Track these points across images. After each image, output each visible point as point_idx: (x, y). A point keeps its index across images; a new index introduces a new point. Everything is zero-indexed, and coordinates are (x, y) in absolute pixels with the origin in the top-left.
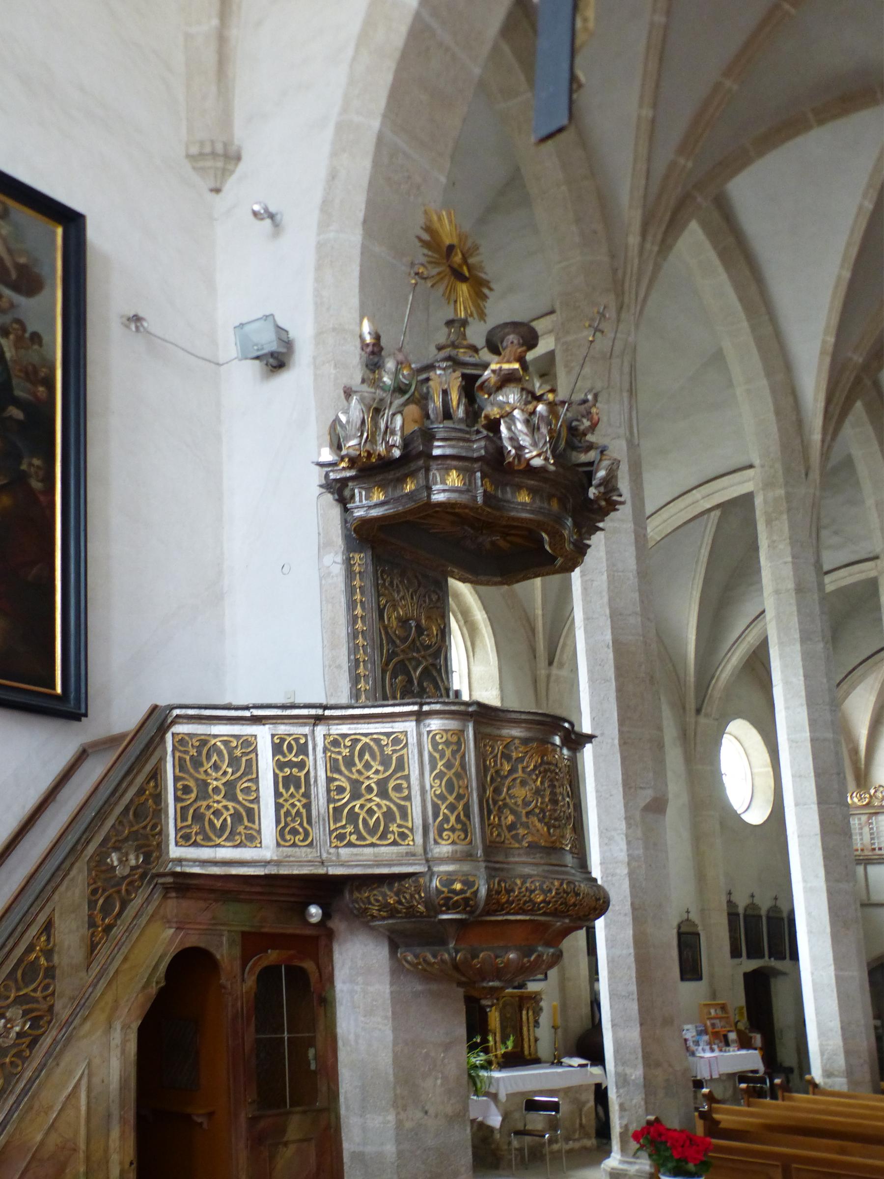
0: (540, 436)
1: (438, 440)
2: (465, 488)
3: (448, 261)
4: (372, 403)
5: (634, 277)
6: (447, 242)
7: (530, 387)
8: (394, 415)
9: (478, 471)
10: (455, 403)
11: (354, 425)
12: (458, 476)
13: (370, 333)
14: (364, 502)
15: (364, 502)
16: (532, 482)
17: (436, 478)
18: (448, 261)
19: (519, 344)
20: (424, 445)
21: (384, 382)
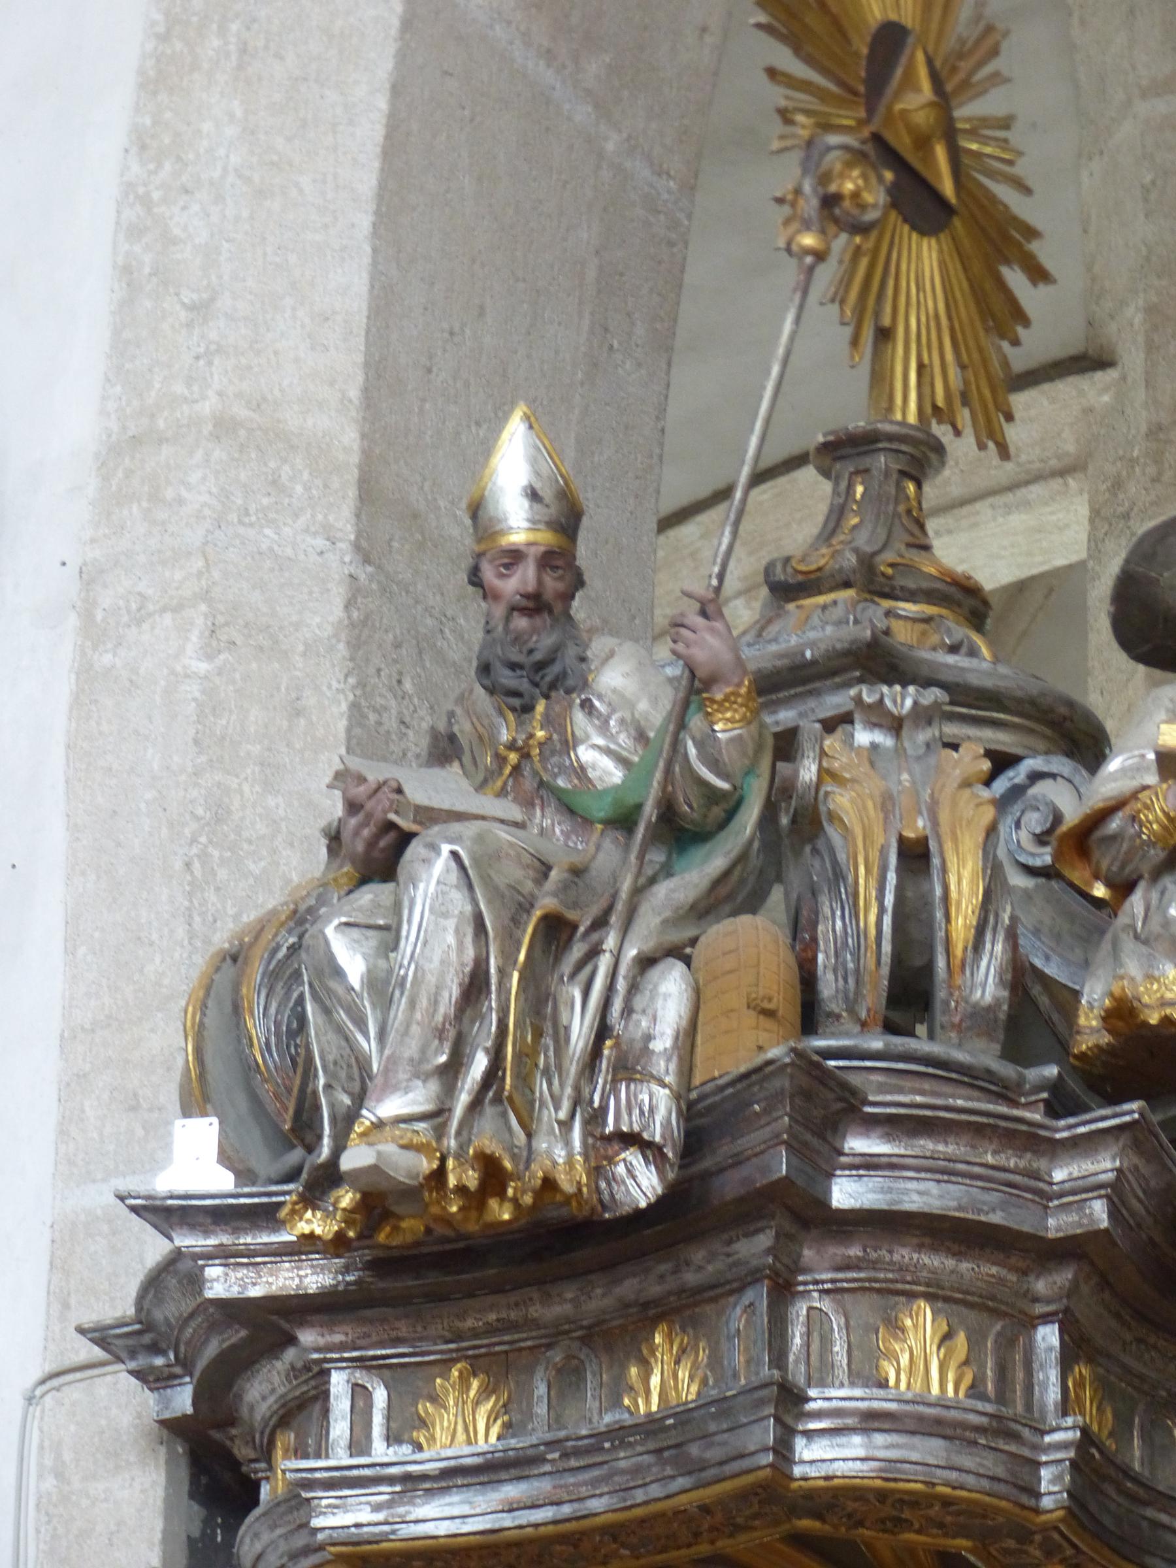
1: (872, 1123)
3: (871, 110)
4: (529, 886)
8: (646, 962)
9: (1046, 1319)
10: (962, 923)
11: (423, 1002)
12: (946, 1338)
13: (533, 495)
14: (380, 1450)
15: (380, 1450)
17: (826, 1342)
18: (871, 110)
20: (796, 1148)
21: (581, 771)
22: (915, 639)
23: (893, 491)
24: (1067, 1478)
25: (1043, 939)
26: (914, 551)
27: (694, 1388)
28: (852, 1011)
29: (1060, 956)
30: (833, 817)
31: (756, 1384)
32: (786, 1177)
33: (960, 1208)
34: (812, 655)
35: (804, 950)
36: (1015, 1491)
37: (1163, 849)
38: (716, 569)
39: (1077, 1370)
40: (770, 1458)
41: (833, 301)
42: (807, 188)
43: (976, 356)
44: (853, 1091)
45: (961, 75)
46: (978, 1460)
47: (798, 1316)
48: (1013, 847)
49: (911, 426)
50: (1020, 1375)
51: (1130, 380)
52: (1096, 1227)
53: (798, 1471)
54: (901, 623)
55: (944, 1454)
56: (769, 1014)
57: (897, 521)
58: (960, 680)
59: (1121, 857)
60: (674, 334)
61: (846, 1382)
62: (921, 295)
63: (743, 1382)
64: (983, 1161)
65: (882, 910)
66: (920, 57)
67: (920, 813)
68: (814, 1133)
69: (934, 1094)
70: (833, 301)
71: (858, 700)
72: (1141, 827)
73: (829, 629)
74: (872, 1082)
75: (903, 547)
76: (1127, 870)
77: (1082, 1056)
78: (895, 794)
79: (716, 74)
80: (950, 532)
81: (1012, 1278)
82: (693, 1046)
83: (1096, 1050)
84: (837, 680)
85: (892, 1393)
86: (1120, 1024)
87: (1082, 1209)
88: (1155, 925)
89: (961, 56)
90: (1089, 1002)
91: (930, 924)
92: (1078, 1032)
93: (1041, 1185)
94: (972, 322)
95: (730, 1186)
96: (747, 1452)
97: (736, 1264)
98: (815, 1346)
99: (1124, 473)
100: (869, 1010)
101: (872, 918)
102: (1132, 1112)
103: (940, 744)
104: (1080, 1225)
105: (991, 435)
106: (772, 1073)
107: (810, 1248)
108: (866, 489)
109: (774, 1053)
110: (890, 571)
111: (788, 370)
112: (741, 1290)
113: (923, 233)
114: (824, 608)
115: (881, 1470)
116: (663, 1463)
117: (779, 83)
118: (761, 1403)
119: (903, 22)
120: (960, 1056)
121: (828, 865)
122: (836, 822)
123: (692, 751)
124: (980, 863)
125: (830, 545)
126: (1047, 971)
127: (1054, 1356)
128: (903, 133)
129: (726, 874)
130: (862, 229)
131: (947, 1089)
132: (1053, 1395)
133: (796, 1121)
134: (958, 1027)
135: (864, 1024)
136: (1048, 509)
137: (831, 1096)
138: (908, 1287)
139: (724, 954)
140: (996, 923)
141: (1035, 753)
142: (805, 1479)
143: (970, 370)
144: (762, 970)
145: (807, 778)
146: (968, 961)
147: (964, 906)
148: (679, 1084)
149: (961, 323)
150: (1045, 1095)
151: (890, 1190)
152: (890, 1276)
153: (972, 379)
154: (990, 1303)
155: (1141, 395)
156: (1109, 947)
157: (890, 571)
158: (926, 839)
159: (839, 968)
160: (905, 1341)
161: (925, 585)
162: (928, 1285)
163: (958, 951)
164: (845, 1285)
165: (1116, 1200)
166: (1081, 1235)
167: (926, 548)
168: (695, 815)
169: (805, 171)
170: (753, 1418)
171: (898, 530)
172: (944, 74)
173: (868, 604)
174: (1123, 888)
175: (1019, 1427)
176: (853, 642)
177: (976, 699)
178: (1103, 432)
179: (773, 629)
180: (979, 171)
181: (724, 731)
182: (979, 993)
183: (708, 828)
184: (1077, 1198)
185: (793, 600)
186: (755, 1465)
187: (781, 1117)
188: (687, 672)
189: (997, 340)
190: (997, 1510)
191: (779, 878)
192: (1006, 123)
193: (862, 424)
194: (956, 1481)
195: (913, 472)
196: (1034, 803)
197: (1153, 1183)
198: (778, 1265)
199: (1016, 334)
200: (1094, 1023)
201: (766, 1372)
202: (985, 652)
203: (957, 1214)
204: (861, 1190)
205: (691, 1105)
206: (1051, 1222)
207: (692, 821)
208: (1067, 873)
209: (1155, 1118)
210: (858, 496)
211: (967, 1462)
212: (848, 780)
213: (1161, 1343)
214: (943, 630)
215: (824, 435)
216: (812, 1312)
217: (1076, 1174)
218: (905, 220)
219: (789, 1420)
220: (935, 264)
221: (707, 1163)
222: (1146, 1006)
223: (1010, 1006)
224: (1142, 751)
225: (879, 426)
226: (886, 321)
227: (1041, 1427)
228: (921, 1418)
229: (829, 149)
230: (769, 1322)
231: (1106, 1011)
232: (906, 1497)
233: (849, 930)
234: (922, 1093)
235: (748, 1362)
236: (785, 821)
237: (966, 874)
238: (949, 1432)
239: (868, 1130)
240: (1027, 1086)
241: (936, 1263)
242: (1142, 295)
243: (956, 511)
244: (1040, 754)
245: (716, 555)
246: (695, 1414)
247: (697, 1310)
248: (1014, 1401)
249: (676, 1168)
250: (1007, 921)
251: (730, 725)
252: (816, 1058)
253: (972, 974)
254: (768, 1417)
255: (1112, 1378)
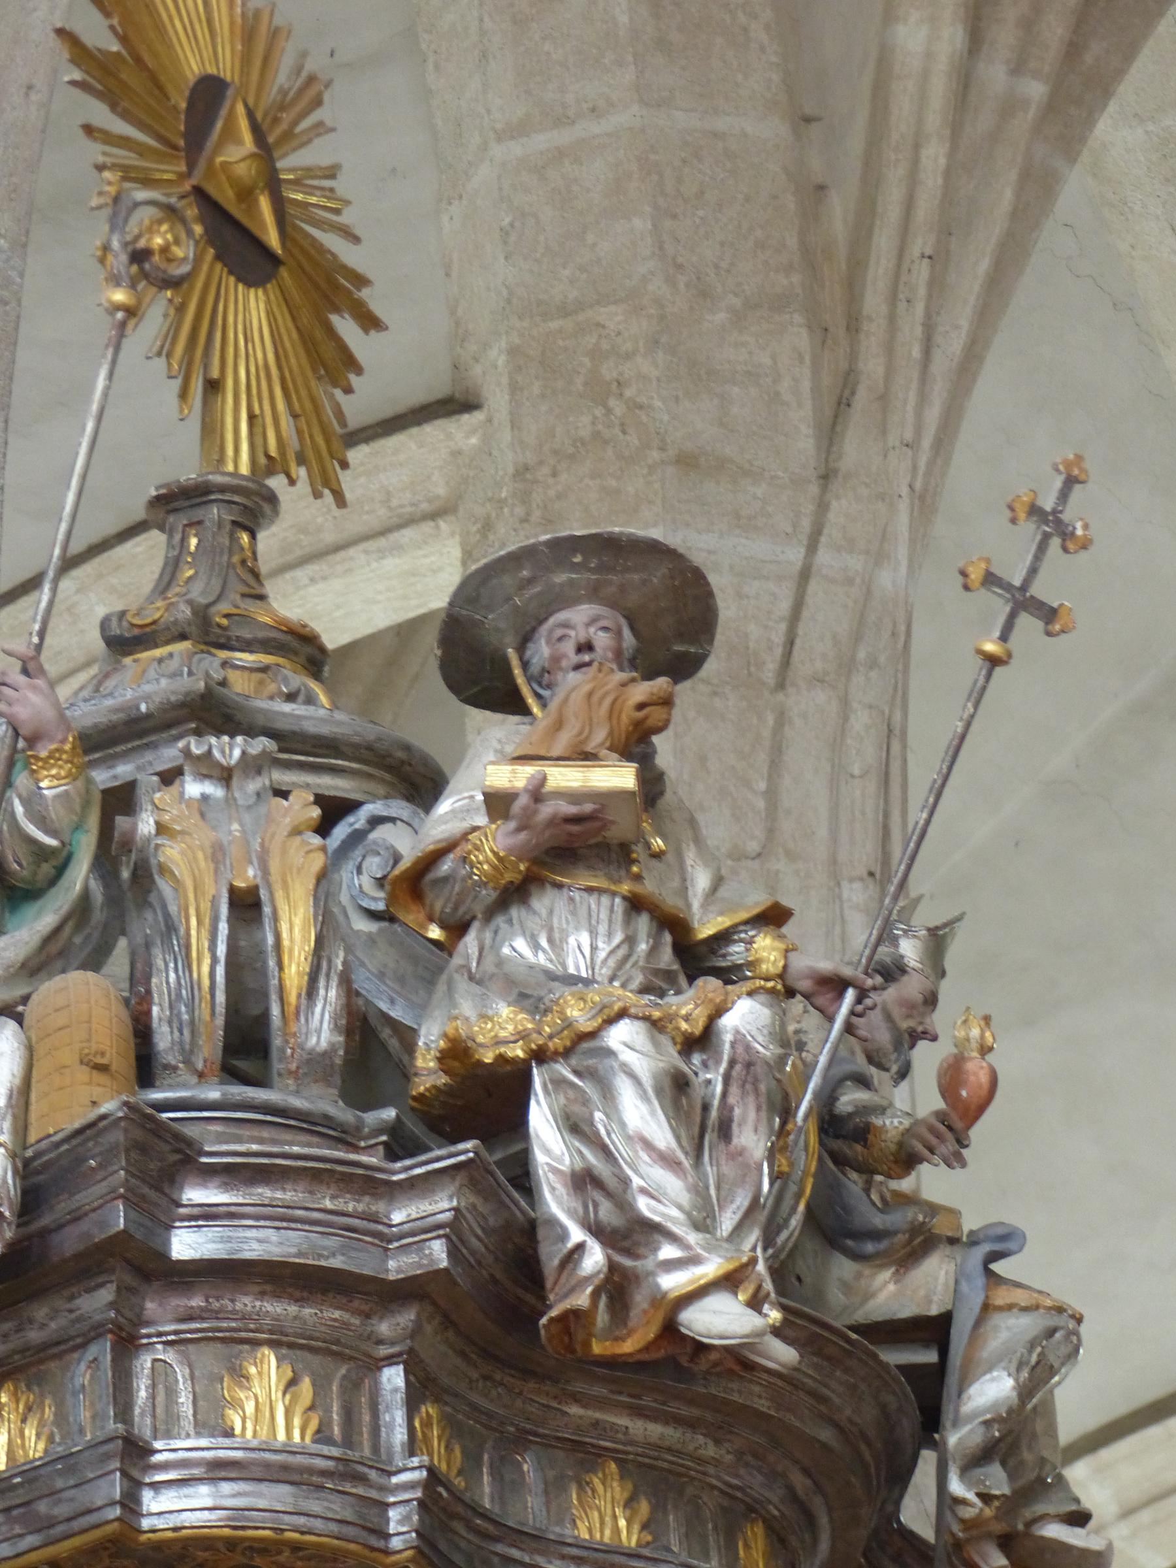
0: (728, 1170)
1: (210, 1173)
2: (324, 1457)
3: (191, 165)
5: (922, 242)
6: (193, 66)
7: (670, 901)
9: (390, 1360)
16: (656, 1430)
17: (172, 1393)
18: (191, 165)
19: (618, 653)
20: (134, 1201)
22: (252, 688)
23: (227, 542)
24: (415, 1518)
25: (388, 982)
26: (249, 601)
27: (41, 1446)
28: (187, 1062)
29: (407, 999)
30: (163, 869)
31: (101, 1439)
32: (124, 1231)
33: (300, 1254)
34: (148, 708)
35: (139, 1004)
36: (364, 1534)
37: (495, 889)
38: (37, 627)
39: (423, 1409)
40: (117, 1511)
41: (159, 354)
42: (116, 244)
43: (308, 405)
44: (189, 1142)
45: (284, 126)
46: (326, 1504)
47: (143, 1369)
48: (355, 892)
49: (243, 477)
50: (367, 1418)
51: (496, 421)
52: (435, 1267)
53: (146, 1523)
54: (238, 673)
55: (291, 1500)
56: (102, 1068)
57: (231, 571)
58: (296, 728)
59: (453, 899)
60: (11, 392)
61: (192, 1433)
62: (250, 346)
63: (88, 1437)
64: (321, 1206)
65: (214, 961)
66: (240, 110)
67: (251, 863)
68: (152, 1187)
69: (274, 1142)
70: (159, 354)
71: (187, 752)
72: (472, 868)
73: (164, 682)
74: (210, 1132)
75: (238, 597)
76: (461, 911)
77: (420, 1098)
78: (226, 843)
79: (43, 131)
80: (324, 578)
81: (355, 1321)
82: (27, 1104)
83: (433, 1091)
84: (174, 732)
85: (237, 1442)
86: (456, 1064)
87: (422, 1250)
88: (489, 965)
89: (282, 107)
90: (425, 1044)
91: (263, 972)
92: (416, 1074)
93: (380, 1227)
94: (303, 374)
95: (69, 1243)
96: (94, 1506)
97: (78, 1320)
98: (161, 1398)
99: (494, 515)
100: (205, 1061)
101: (206, 969)
102: (466, 1151)
103: (270, 793)
104: (420, 1266)
105: (326, 483)
106: (106, 1129)
107: (152, 1301)
108: (199, 541)
109: (107, 1107)
110: (225, 622)
111: (103, 424)
112: (84, 1346)
113: (249, 284)
114: (160, 661)
115: (229, 1519)
116: (11, 1521)
117: (95, 139)
118: (107, 1457)
119: (222, 75)
120: (297, 1103)
121: (161, 918)
122: (167, 875)
123: (19, 809)
124: (312, 910)
125: (165, 599)
126: (392, 1014)
127: (400, 1397)
128: (226, 186)
129: (57, 931)
130: (174, 283)
131: (287, 1136)
132: (400, 1435)
133: (133, 1175)
134: (294, 1074)
135: (201, 1075)
136: (421, 553)
137: (166, 1148)
138: (251, 1335)
139: (57, 1010)
140: (329, 968)
141: (374, 798)
142: (154, 1531)
143: (303, 419)
144: (94, 1026)
145: (146, 831)
146: (303, 1007)
147: (296, 953)
148: (14, 1142)
149: (291, 372)
150: (384, 1138)
151: (229, 1240)
152: (234, 1325)
153: (305, 428)
154: (334, 1347)
155: (506, 435)
156: (445, 987)
157: (225, 622)
158: (256, 888)
159: (173, 1019)
160: (250, 1389)
161: (261, 634)
162: (271, 1332)
163: (292, 998)
164: (189, 1336)
165: (454, 1238)
166: (420, 1275)
167: (261, 597)
168: (25, 873)
169: (113, 228)
170: (100, 1473)
171: (233, 581)
172: (265, 127)
173: (205, 655)
174: (457, 929)
175: (366, 1470)
176: (187, 694)
177: (314, 746)
178: (472, 474)
179: (110, 683)
180: (302, 221)
181: (49, 788)
182: (314, 1040)
183: (39, 885)
184: (416, 1239)
185: (130, 654)
186: (103, 1520)
187: (116, 1172)
188: (10, 731)
189: (330, 389)
190: (347, 1553)
191: (123, 933)
192: (332, 172)
193: (193, 476)
194: (304, 1526)
195: (248, 523)
196: (374, 847)
197: (492, 1221)
198: (121, 1319)
199: (347, 379)
200: (432, 1064)
201: (113, 1426)
202: (323, 699)
203: (297, 1260)
204: (200, 1241)
205: (27, 1163)
206: (392, 1264)
207: (23, 880)
208: (401, 916)
209: (492, 1158)
210: (192, 548)
211: (315, 1507)
212: (180, 832)
213: (507, 1379)
214: (280, 678)
215: (157, 489)
216: (157, 1364)
217: (414, 1216)
218: (231, 272)
219: (135, 1473)
220: (263, 315)
221: (46, 1220)
222: (481, 1045)
223: (347, 1052)
224: (472, 793)
225: (210, 477)
226: (215, 374)
227: (388, 1468)
228: (267, 1465)
229: (137, 205)
230: (113, 1376)
231: (441, 1052)
232: (256, 1545)
233: (183, 982)
234: (261, 1141)
235: (94, 1417)
236: (125, 874)
237: (298, 921)
238: (297, 1478)
239: (205, 1181)
240: (366, 1130)
241: (279, 1310)
242: (504, 337)
243: (330, 557)
244: (379, 799)
245: (36, 614)
246: (42, 1471)
247: (42, 1367)
248: (361, 1443)
249: (14, 1227)
250: (340, 967)
251: (56, 782)
252: (149, 1111)
253: (307, 1020)
254: (113, 1472)
255: (460, 1417)
